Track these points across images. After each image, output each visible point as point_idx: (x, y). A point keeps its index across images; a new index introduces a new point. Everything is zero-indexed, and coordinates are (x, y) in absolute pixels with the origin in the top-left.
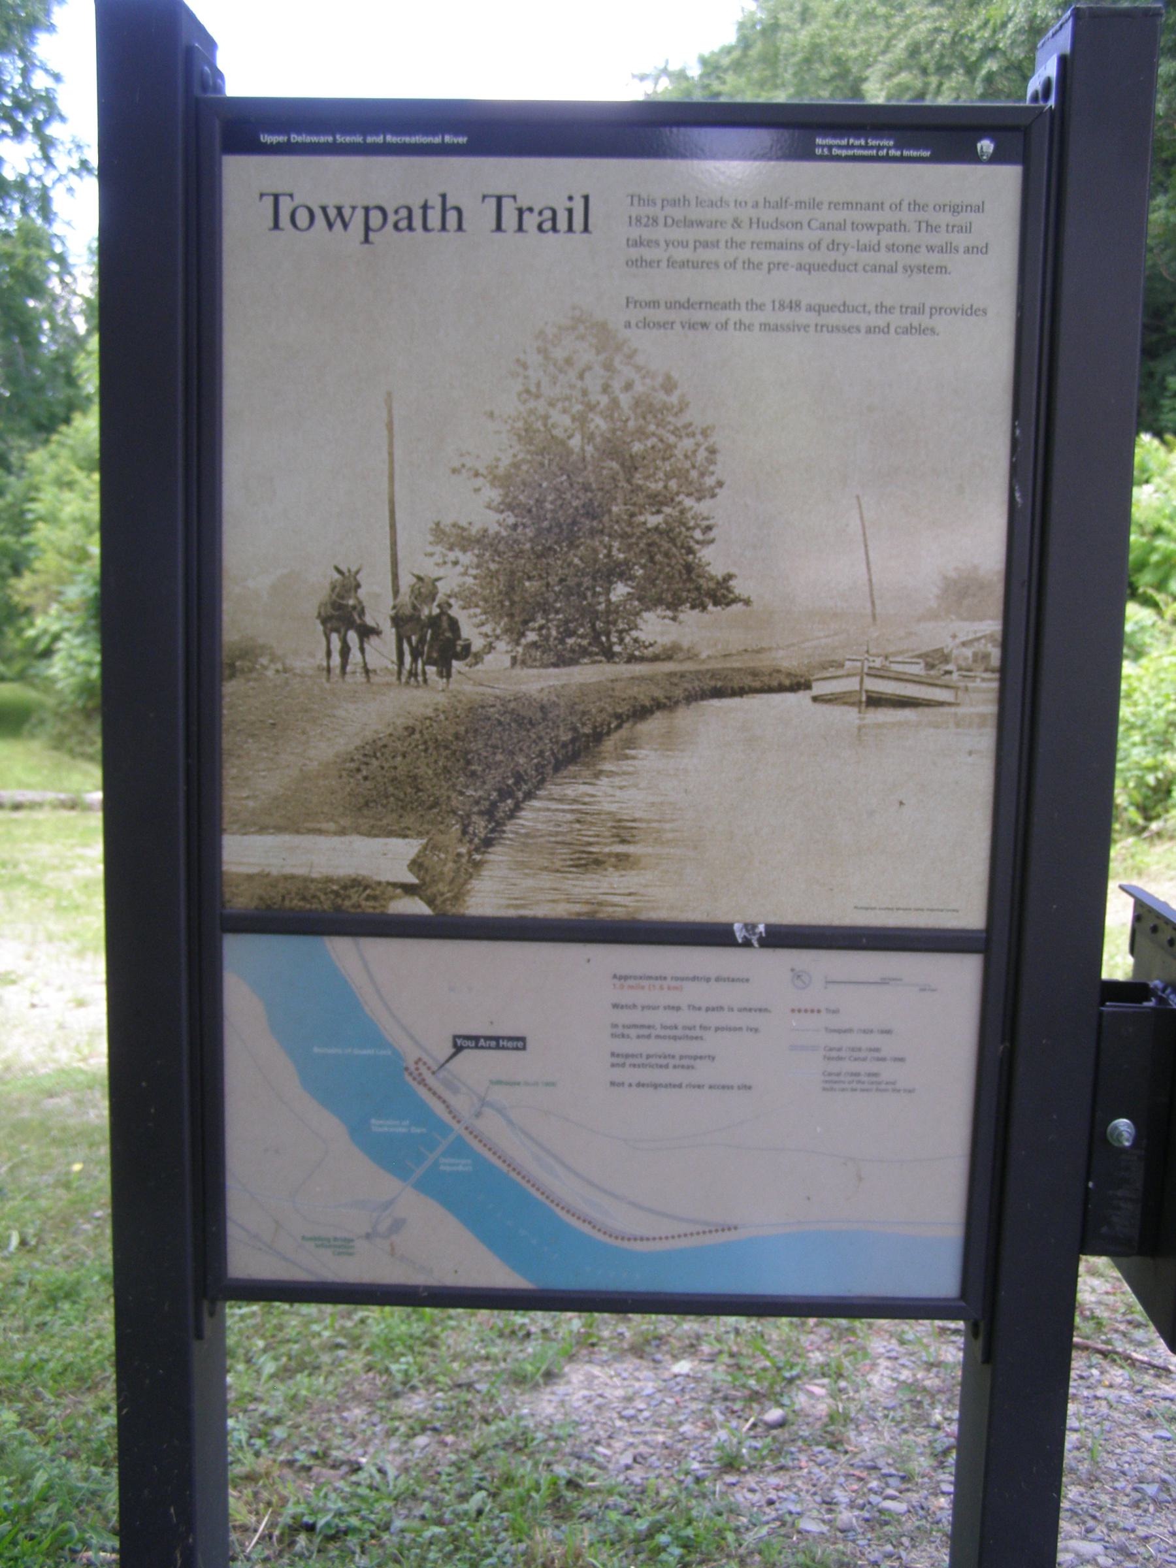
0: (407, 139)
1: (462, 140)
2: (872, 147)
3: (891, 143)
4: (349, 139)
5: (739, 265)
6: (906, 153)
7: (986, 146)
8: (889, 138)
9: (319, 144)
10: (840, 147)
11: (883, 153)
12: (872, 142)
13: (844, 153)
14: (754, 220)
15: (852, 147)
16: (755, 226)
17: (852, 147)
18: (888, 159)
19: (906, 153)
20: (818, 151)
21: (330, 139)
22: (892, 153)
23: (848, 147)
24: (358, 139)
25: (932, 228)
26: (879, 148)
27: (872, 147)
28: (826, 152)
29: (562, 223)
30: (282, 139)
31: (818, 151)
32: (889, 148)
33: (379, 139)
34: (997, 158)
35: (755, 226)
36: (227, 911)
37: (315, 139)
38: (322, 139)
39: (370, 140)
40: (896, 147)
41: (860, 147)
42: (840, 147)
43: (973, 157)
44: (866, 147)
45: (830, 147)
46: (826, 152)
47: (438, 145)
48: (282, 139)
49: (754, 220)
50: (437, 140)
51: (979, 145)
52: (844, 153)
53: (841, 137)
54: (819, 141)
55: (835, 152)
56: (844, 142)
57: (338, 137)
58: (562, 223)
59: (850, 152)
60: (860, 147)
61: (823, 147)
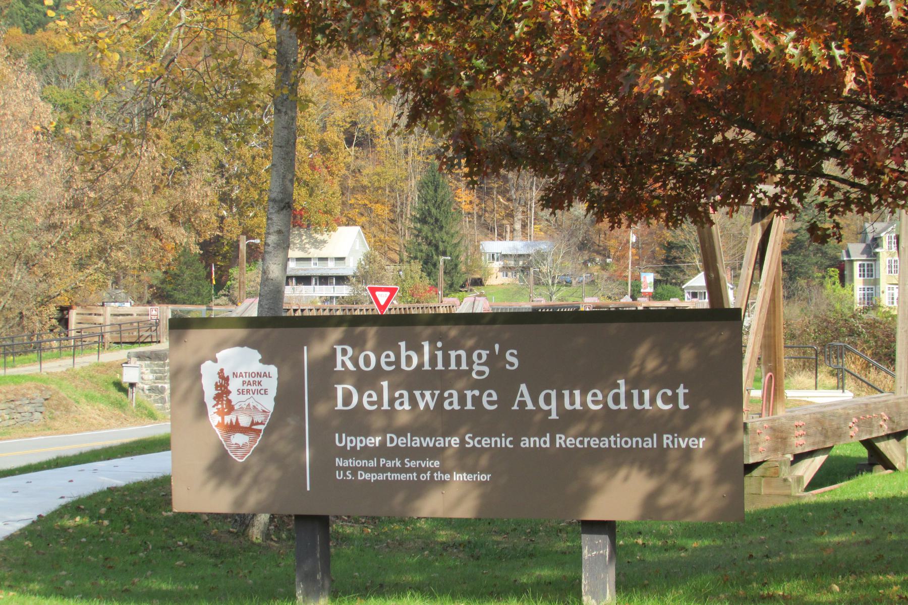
1: (337, 435)
2: (410, 470)
15: (384, 470)
17: (384, 470)
27: (410, 470)
32: (433, 470)
41: (394, 470)
42: (367, 470)
60: (394, 470)
61: (345, 469)
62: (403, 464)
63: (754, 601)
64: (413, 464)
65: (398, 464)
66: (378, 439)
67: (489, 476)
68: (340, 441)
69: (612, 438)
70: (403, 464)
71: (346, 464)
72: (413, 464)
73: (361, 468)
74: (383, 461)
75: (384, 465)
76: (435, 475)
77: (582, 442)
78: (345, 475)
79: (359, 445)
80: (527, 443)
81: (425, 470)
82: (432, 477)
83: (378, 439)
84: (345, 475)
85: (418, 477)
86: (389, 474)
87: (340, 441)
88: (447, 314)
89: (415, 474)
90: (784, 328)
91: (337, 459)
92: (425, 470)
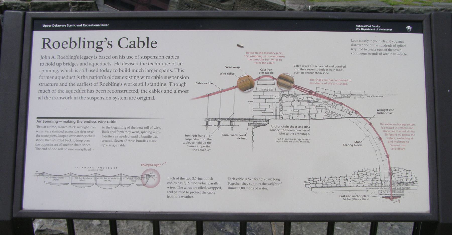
0: (90, 25)
1: (107, 25)
2: (373, 28)
3: (380, 27)
4: (71, 26)
5: (57, 91)
6: (384, 30)
7: (409, 28)
8: (379, 25)
9: (91, 27)
10: (363, 28)
11: (377, 29)
12: (373, 26)
13: (365, 29)
14: (116, 63)
15: (367, 28)
16: (116, 64)
17: (367, 28)
18: (378, 31)
19: (384, 30)
20: (357, 29)
21: (65, 26)
22: (380, 29)
23: (366, 28)
24: (74, 25)
25: (118, 64)
26: (376, 28)
27: (373, 28)
28: (359, 29)
29: (180, 64)
30: (50, 26)
31: (357, 29)
32: (379, 28)
33: (81, 25)
34: (412, 31)
35: (116, 64)
36: (429, 212)
37: (60, 26)
38: (63, 26)
39: (78, 26)
40: (381, 28)
41: (370, 28)
42: (363, 28)
43: (406, 31)
44: (372, 28)
45: (360, 28)
46: (359, 29)
47: (99, 27)
48: (50, 26)
49: (116, 63)
50: (99, 25)
51: (407, 27)
52: (365, 29)
53: (364, 25)
54: (357, 26)
55: (362, 29)
56: (365, 26)
57: (67, 25)
58: (180, 64)
59: (367, 29)
60: (370, 28)
61: (358, 28)
62: (372, 26)
63: (398, 124)
64: (374, 26)
65: (371, 26)
66: (51, 25)
67: (108, 25)
68: (44, 26)
69: (93, 25)
70: (372, 26)
71: (358, 26)
72: (374, 26)
73: (362, 27)
74: (367, 26)
75: (367, 27)
76: (379, 29)
77: (87, 25)
78: (358, 29)
79: (45, 27)
80: (65, 26)
81: (377, 28)
82: (379, 29)
83: (51, 25)
84: (358, 29)
85: (375, 29)
86: (369, 29)
87: (44, 26)
88: (103, 26)
89: (375, 29)
90: (197, 10)
91: (356, 25)
92: (377, 28)
